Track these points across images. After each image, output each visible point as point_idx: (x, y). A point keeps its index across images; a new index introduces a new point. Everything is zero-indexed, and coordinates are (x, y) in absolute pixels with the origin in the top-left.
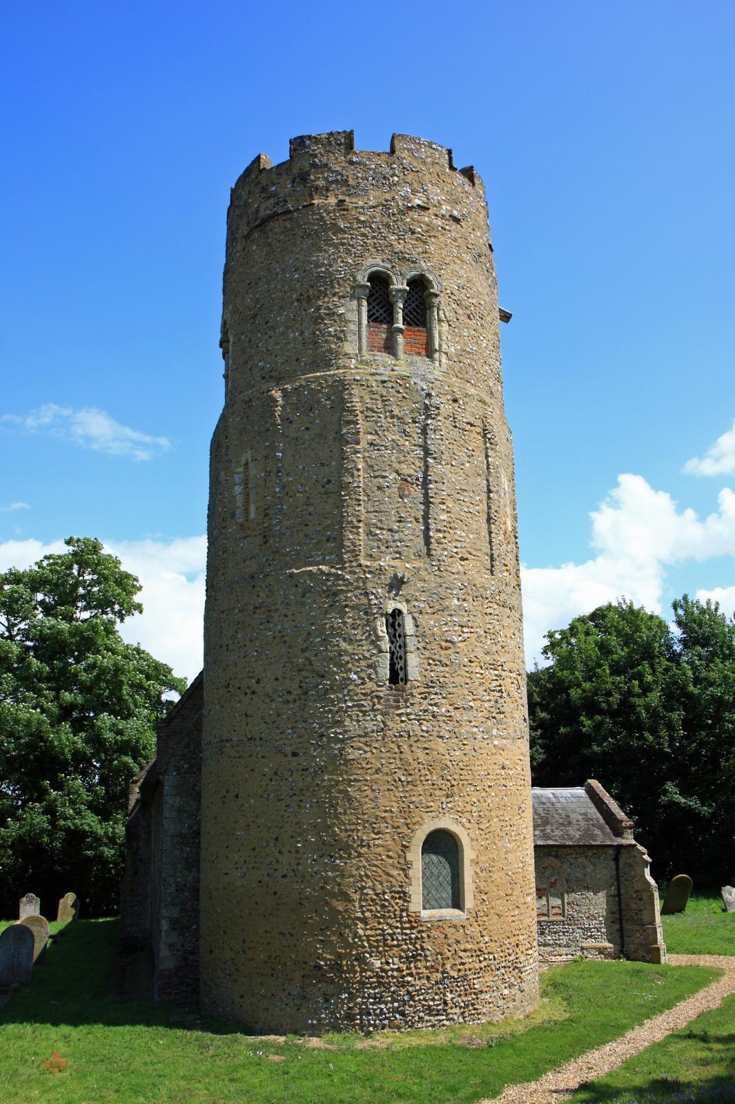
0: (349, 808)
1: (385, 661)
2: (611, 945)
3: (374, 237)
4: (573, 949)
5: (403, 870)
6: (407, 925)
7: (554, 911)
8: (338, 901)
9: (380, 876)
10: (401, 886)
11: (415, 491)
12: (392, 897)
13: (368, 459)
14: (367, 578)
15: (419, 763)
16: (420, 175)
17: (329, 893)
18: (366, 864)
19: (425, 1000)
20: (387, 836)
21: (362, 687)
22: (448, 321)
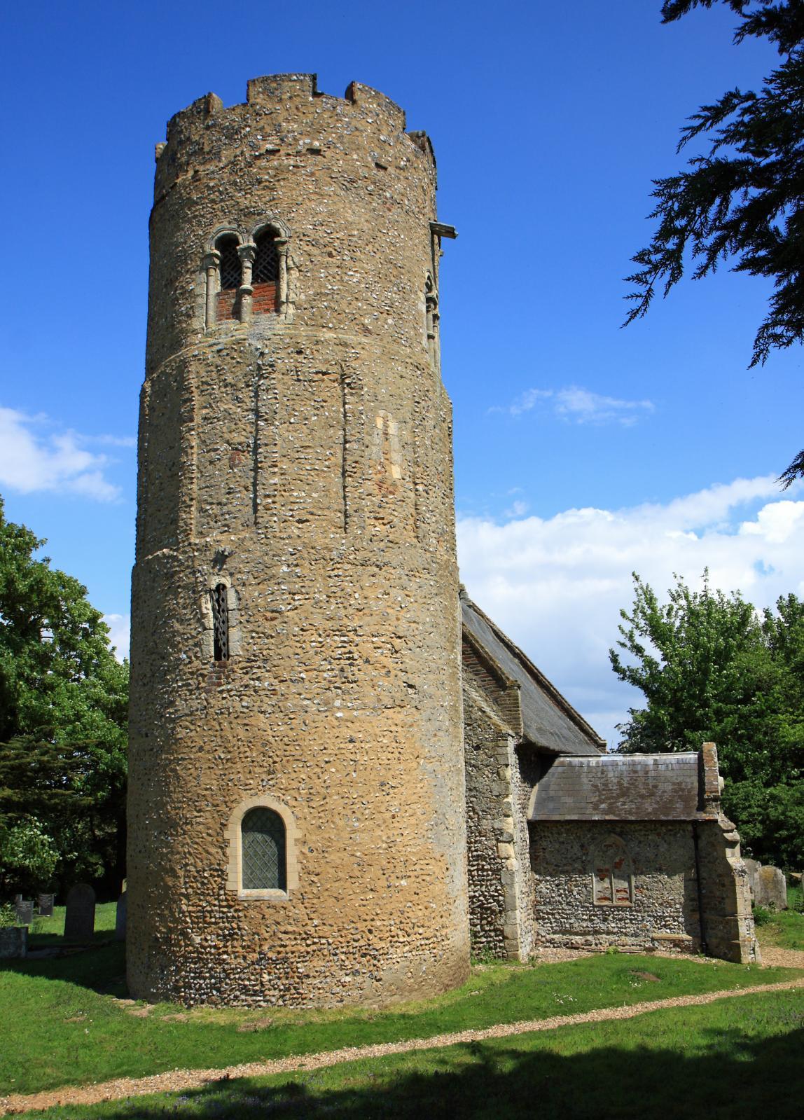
0: (178, 786)
1: (209, 639)
2: (689, 937)
3: (222, 200)
4: (642, 939)
5: (222, 848)
6: (224, 903)
7: (620, 895)
8: (169, 876)
9: (201, 854)
10: (219, 865)
11: (246, 458)
12: (211, 875)
13: (201, 435)
14: (195, 556)
15: (238, 740)
16: (274, 115)
17: (164, 869)
18: (189, 841)
19: (240, 978)
20: (207, 814)
21: (189, 666)
22: (297, 267)
